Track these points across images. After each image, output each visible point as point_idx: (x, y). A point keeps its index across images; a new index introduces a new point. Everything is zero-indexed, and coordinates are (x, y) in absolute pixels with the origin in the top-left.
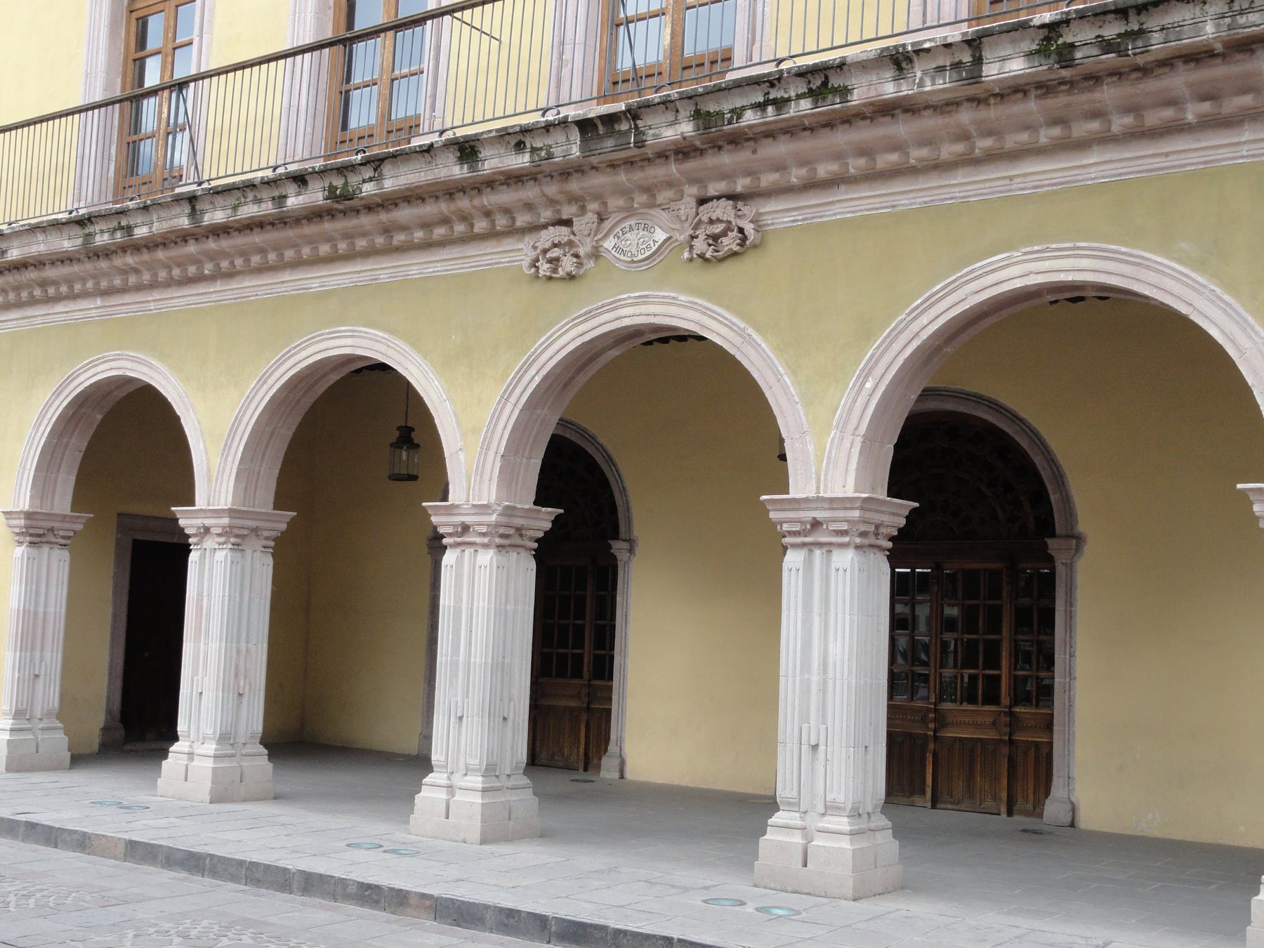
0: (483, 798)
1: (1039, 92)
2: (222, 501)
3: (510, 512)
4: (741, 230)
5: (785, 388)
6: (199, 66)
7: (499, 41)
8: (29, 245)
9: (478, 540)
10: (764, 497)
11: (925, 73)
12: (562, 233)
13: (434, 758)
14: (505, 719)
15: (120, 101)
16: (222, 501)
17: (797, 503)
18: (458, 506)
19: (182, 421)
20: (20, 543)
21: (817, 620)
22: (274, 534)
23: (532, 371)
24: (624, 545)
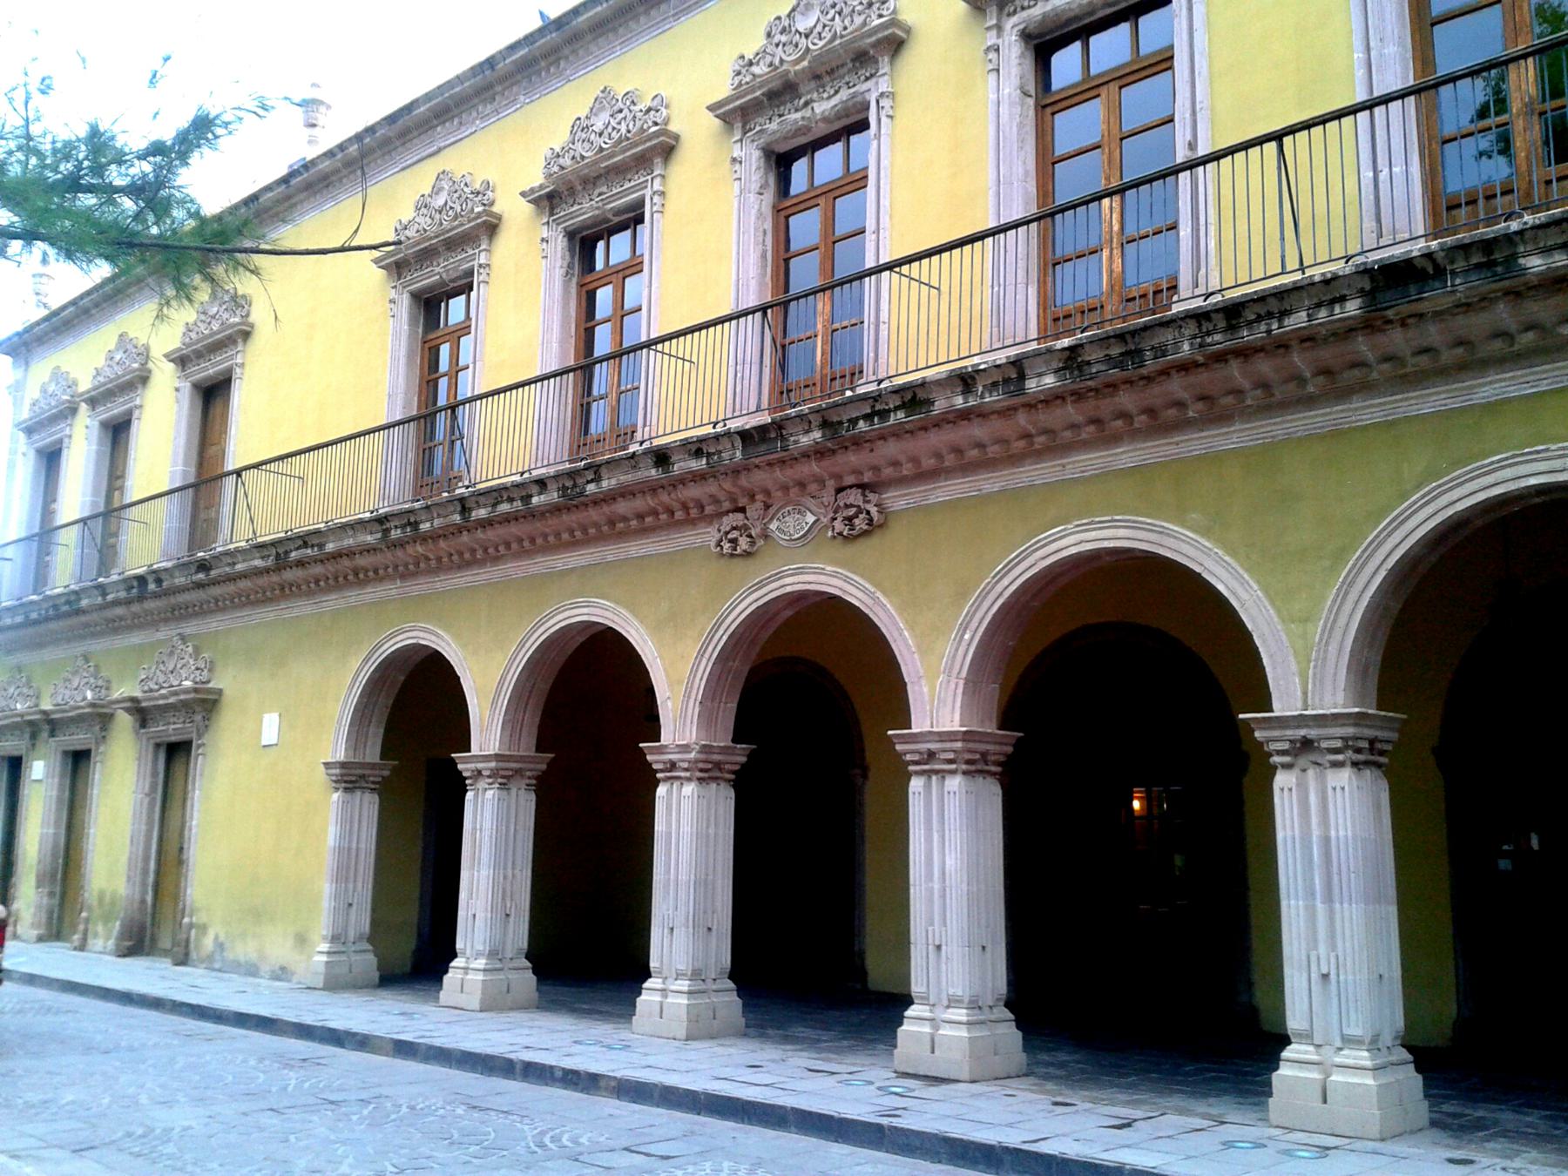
0: (969, 1031)
1: (1073, 398)
2: (491, 747)
3: (707, 750)
4: (868, 513)
5: (905, 639)
6: (649, 335)
7: (938, 289)
8: (341, 539)
9: (683, 774)
10: (890, 732)
11: (984, 386)
12: (737, 519)
13: (652, 965)
14: (709, 929)
15: (1038, 219)
16: (491, 747)
17: (915, 738)
18: (666, 746)
19: (462, 680)
20: (337, 789)
21: (936, 836)
22: (535, 773)
23: (721, 632)
24: (857, 771)
